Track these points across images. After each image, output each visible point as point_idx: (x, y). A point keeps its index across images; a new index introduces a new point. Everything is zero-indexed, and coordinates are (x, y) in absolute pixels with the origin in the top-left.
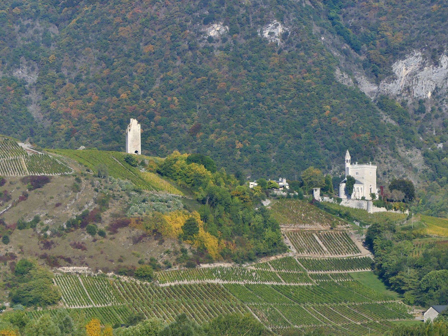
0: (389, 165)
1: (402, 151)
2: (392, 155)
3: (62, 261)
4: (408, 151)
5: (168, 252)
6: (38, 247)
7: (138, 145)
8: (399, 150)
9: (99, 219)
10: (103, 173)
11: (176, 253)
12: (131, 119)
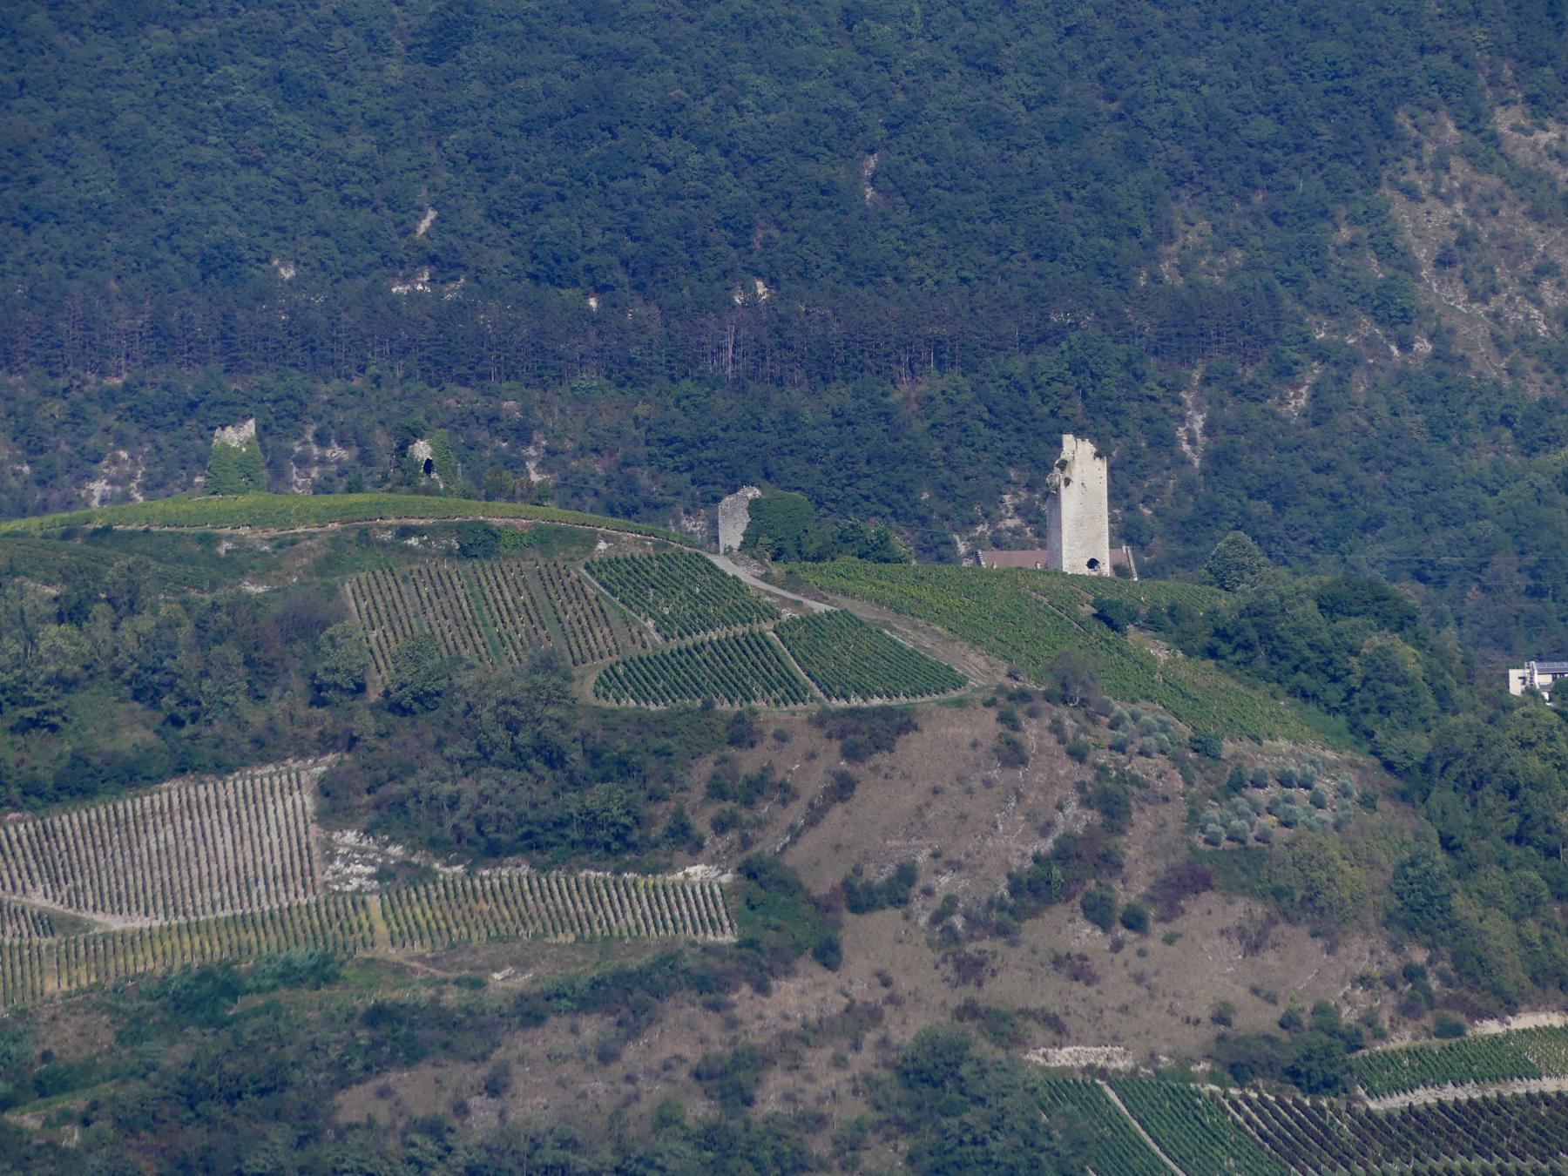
0: (1459, 207)
1: (1516, 128)
2: (1469, 155)
3: (1039, 1033)
4: (1547, 130)
5: (1364, 981)
6: (937, 975)
7: (1099, 536)
8: (1504, 120)
9: (1109, 863)
10: (1077, 691)
11: (1391, 983)
12: (1068, 440)
